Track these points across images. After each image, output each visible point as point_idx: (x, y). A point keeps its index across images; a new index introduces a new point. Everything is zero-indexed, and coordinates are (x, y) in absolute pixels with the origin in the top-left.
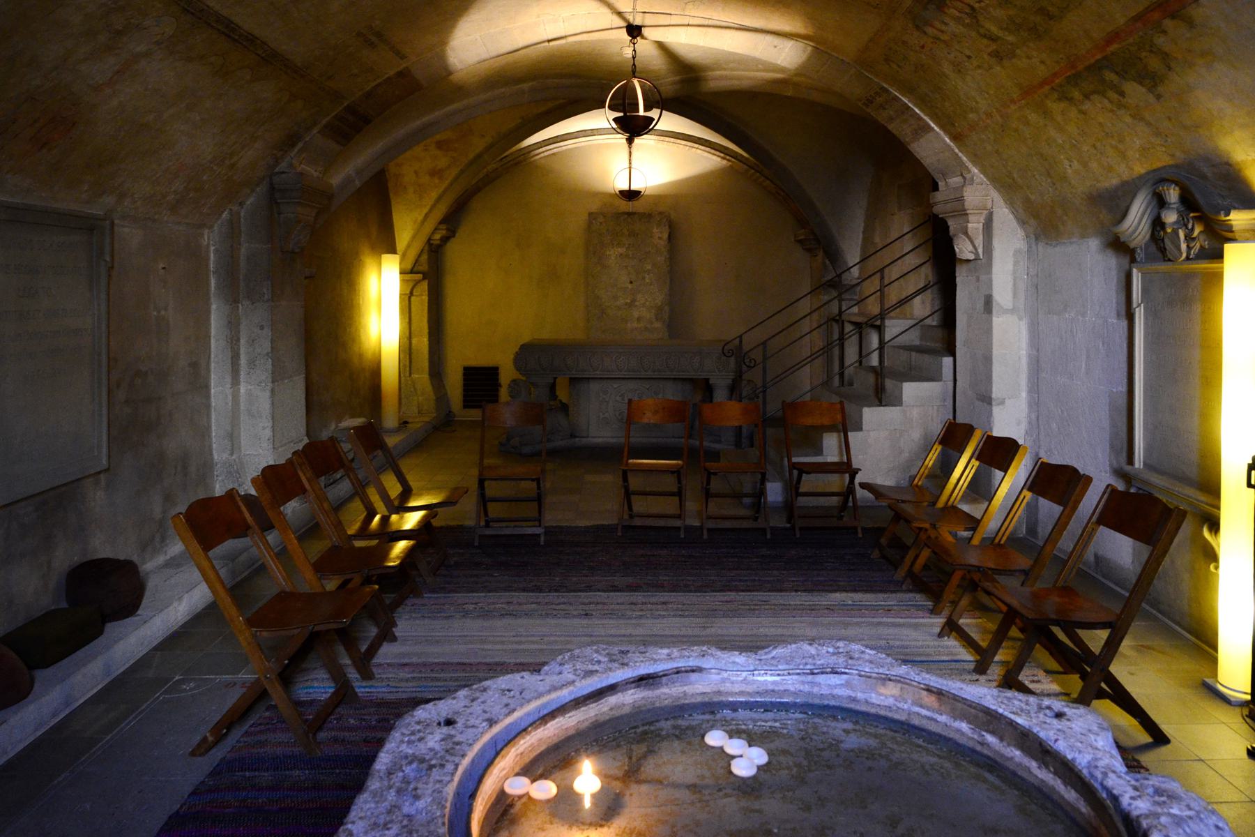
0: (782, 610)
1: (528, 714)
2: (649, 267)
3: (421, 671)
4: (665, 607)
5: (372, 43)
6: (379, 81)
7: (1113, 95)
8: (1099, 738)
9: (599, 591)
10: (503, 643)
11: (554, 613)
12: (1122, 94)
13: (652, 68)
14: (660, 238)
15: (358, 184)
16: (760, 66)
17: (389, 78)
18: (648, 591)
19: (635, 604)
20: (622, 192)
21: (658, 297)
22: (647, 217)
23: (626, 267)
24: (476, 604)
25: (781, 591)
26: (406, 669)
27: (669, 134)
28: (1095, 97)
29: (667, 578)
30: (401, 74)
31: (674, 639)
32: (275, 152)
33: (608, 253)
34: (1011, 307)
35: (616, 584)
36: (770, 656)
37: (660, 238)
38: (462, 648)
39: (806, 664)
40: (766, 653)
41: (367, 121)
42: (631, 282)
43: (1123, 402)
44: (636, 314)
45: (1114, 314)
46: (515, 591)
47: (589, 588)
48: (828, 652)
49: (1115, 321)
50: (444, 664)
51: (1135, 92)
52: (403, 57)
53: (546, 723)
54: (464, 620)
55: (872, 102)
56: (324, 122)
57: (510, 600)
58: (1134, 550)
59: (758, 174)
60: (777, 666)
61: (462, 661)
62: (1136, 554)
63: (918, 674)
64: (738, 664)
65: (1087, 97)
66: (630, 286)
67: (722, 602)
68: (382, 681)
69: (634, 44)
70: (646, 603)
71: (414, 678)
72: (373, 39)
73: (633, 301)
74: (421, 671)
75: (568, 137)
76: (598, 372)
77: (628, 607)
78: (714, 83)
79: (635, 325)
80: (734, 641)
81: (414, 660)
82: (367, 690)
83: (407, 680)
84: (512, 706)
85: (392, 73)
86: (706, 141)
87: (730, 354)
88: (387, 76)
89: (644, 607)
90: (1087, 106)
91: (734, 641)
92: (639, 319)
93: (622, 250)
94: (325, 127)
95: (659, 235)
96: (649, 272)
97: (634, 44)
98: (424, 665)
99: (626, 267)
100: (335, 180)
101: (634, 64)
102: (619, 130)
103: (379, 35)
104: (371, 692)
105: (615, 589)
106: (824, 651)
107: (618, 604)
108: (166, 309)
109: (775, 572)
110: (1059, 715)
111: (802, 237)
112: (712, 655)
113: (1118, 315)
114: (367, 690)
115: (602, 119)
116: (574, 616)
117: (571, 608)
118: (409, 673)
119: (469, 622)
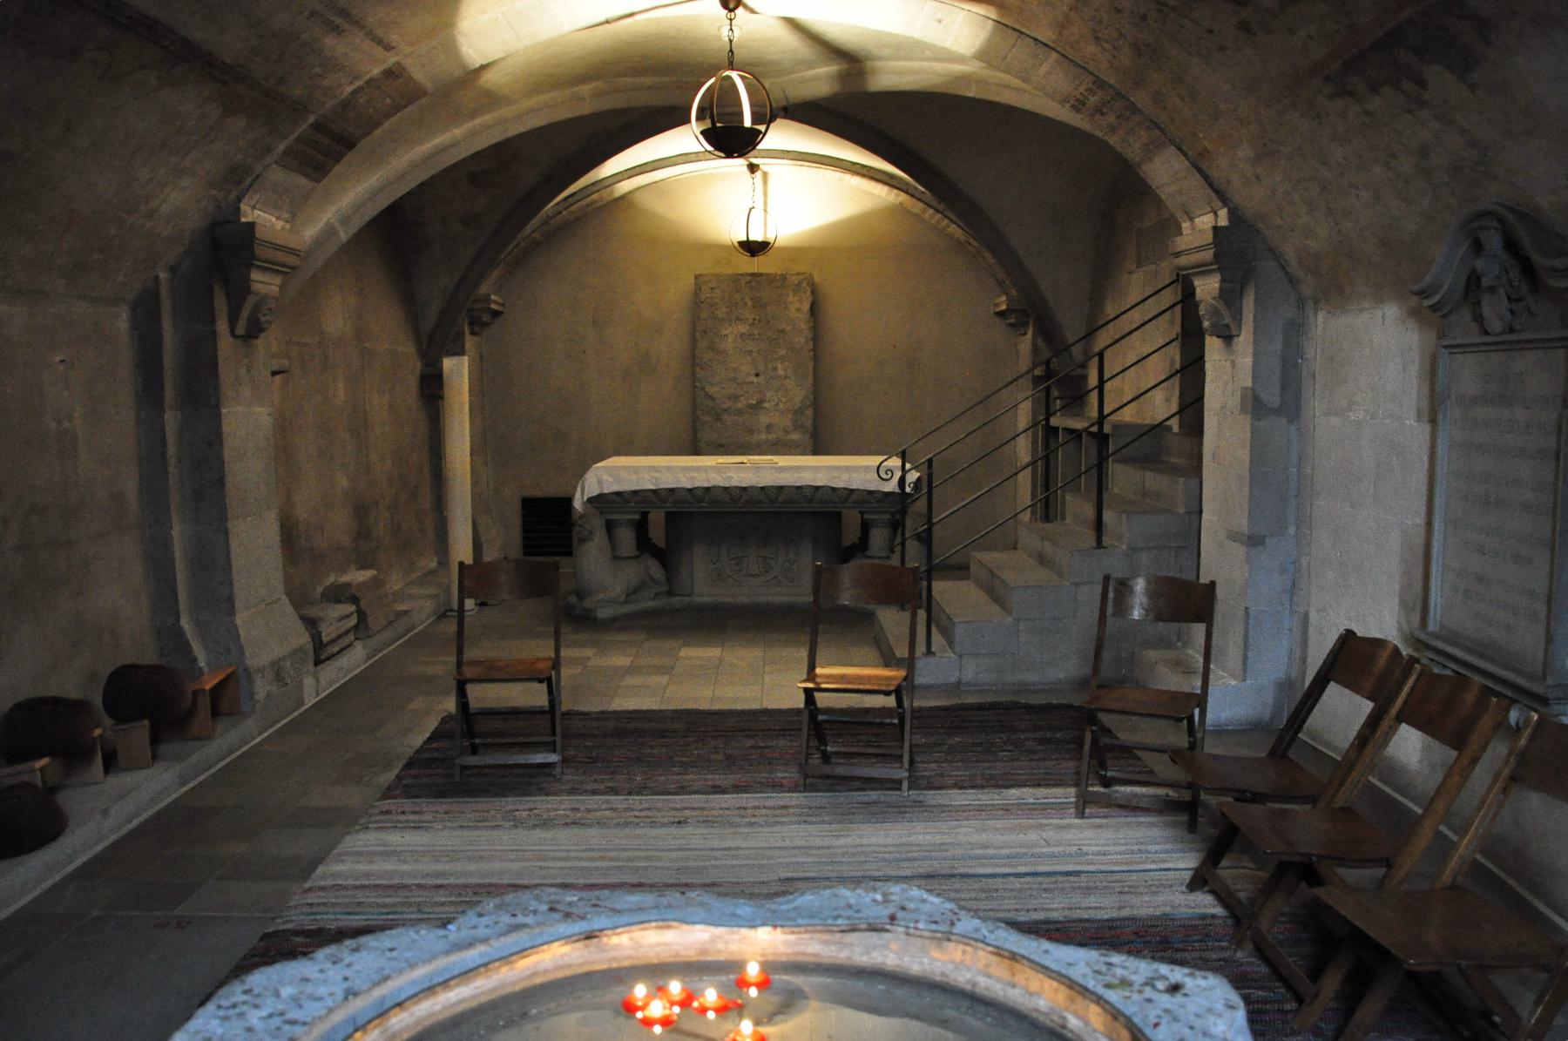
0: (942, 812)
1: (413, 982)
2: (782, 352)
3: (460, 894)
4: (785, 811)
5: (338, 27)
6: (359, 83)
7: (1408, 86)
8: (1219, 1021)
9: (695, 793)
10: (565, 859)
11: (637, 820)
12: (1422, 83)
13: (770, 57)
14: (798, 310)
15: (344, 236)
16: (928, 53)
17: (371, 80)
18: (761, 792)
19: (745, 808)
20: (741, 243)
21: (798, 393)
22: (776, 282)
23: (750, 353)
24: (530, 810)
25: (940, 788)
26: (441, 892)
27: (813, 158)
28: (1386, 90)
29: (787, 775)
30: (390, 73)
31: (797, 852)
32: (214, 192)
33: (723, 332)
34: (1276, 406)
35: (718, 783)
36: (791, 906)
37: (798, 310)
38: (515, 866)
39: (838, 917)
40: (788, 902)
41: (349, 144)
42: (757, 375)
43: (1419, 540)
44: (764, 420)
45: (1413, 414)
46: (581, 794)
47: (682, 790)
48: (874, 901)
49: (1415, 424)
50: (490, 885)
51: (1440, 78)
52: (388, 48)
53: (434, 994)
54: (514, 831)
55: (1084, 104)
56: (281, 147)
57: (576, 806)
58: (1424, 743)
59: (939, 215)
60: (794, 920)
61: (515, 882)
62: (1426, 749)
63: (992, 932)
64: (740, 916)
65: (1374, 88)
66: (755, 380)
67: (862, 803)
68: (411, 906)
69: (731, 20)
70: (759, 808)
71: (451, 902)
72: (338, 20)
73: (761, 402)
74: (460, 894)
75: (665, 163)
76: (704, 504)
77: (736, 812)
78: (889, 77)
79: (763, 436)
80: (876, 852)
81: (452, 881)
82: (390, 917)
83: (443, 904)
84: (386, 972)
85: (376, 71)
86: (870, 168)
87: (884, 476)
88: (368, 77)
89: (757, 812)
90: (1376, 103)
91: (876, 852)
92: (769, 428)
93: (743, 328)
94: (286, 153)
95: (797, 307)
96: (782, 359)
97: (731, 20)
98: (466, 886)
99: (750, 353)
100: (310, 232)
101: (731, 51)
102: (717, 153)
103: (343, 13)
104: (395, 920)
105: (718, 790)
106: (868, 899)
107: (721, 809)
108: (70, 418)
109: (934, 766)
110: (1175, 988)
111: (1004, 307)
112: (702, 904)
113: (1419, 412)
114: (390, 917)
115: (686, 138)
116: (663, 825)
117: (658, 814)
118: (446, 896)
119: (521, 834)
